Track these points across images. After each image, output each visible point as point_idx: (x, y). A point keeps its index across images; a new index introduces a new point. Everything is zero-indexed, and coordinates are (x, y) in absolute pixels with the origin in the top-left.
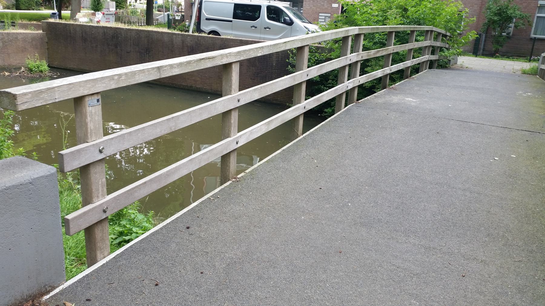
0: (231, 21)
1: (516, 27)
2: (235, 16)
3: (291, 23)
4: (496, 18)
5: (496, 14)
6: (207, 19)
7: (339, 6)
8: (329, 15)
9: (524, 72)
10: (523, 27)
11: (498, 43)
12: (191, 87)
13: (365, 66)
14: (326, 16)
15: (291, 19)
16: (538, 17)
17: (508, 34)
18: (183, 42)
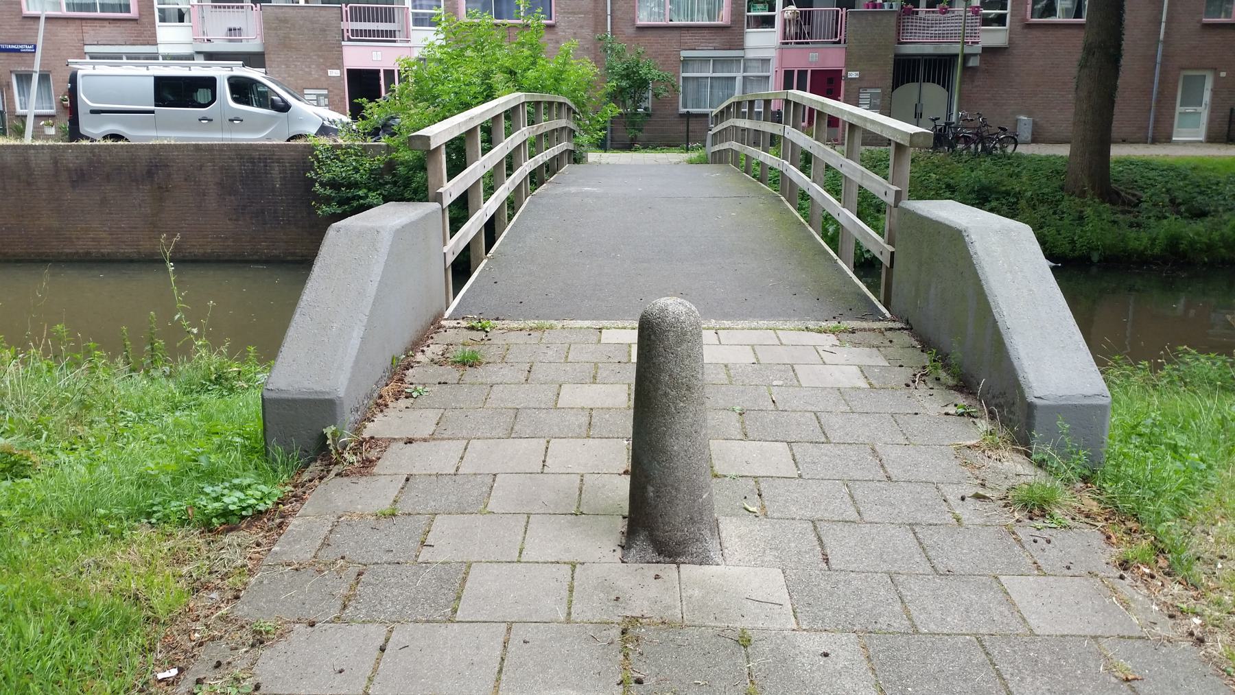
0: (152, 112)
1: (656, 95)
2: (160, 100)
3: (285, 107)
4: (624, 84)
5: (622, 77)
6: (93, 112)
7: (342, 73)
8: (325, 92)
9: (691, 162)
10: (666, 94)
11: (633, 124)
12: (88, 253)
13: (536, 145)
14: (318, 95)
15: (283, 100)
16: (1185, 77)
17: (645, 109)
18: (56, 162)
